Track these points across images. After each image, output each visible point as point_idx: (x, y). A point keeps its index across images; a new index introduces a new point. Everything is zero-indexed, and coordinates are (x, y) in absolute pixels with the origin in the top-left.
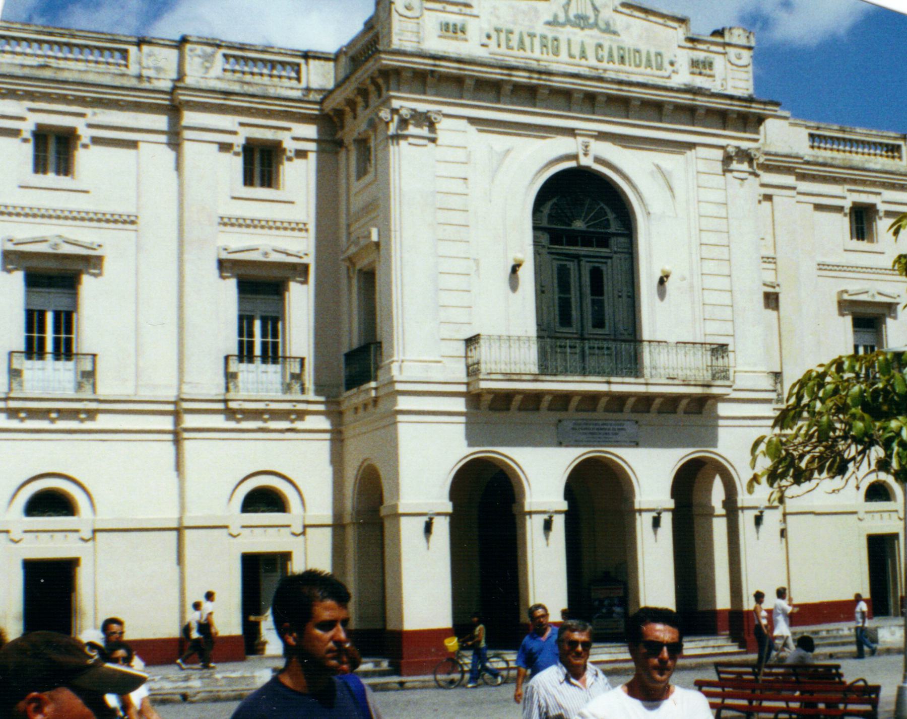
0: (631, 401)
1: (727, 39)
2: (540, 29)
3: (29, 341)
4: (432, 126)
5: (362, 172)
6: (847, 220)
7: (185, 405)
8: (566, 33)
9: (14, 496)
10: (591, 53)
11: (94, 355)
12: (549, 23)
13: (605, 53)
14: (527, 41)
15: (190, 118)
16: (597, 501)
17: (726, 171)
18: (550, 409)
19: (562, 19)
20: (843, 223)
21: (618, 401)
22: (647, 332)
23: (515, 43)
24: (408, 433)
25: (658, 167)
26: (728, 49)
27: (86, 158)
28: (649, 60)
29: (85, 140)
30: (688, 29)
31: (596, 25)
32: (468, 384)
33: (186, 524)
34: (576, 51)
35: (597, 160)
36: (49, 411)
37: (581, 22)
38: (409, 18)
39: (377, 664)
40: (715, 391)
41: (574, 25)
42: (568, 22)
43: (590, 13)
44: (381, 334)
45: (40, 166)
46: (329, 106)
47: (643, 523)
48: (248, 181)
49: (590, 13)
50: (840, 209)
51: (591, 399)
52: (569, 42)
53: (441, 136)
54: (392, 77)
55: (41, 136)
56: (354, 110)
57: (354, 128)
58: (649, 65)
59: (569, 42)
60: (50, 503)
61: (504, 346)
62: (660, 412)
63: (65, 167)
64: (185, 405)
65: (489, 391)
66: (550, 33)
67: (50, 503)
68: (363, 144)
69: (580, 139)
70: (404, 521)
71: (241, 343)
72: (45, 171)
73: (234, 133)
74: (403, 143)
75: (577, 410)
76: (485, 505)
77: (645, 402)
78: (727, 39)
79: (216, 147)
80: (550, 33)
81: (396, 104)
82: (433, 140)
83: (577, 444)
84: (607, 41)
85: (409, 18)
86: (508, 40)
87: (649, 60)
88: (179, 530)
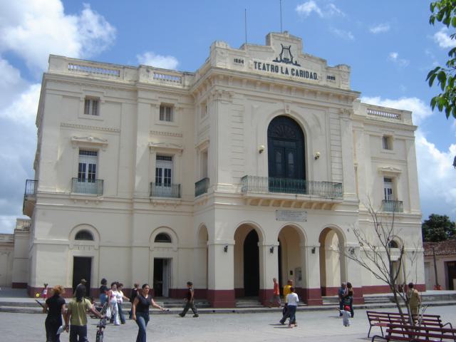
0: (261, 201)
1: (340, 69)
2: (271, 63)
3: (80, 175)
4: (230, 96)
5: (203, 115)
6: (382, 141)
7: (136, 200)
8: (280, 65)
9: (77, 226)
10: (290, 72)
11: (103, 181)
12: (274, 61)
13: (295, 72)
14: (266, 66)
15: (141, 94)
16: (290, 239)
17: (339, 119)
18: (273, 206)
19: (279, 59)
20: (381, 142)
21: (300, 204)
22: (310, 177)
23: (261, 67)
24: (218, 213)
25: (314, 115)
26: (341, 73)
27: (103, 108)
28: (311, 75)
29: (103, 102)
30: (326, 64)
31: (291, 62)
32: (242, 195)
33: (134, 245)
34: (284, 71)
35: (292, 111)
36: (85, 200)
37: (286, 61)
38: (173, 230)
39: (204, 303)
40: (334, 201)
41: (283, 62)
42: (281, 61)
43: (289, 57)
44: (210, 176)
45: (86, 112)
46: (192, 91)
47: (308, 251)
48: (161, 118)
49: (289, 57)
50: (379, 137)
51: (289, 203)
52: (282, 68)
53: (234, 101)
54: (216, 77)
55: (87, 101)
56: (201, 92)
57: (201, 99)
58: (311, 77)
59: (282, 68)
60: (84, 235)
61: (261, 181)
62: (315, 208)
63: (96, 112)
64: (136, 200)
65: (250, 197)
66: (275, 64)
67: (84, 235)
68: (204, 104)
69: (286, 104)
70: (216, 247)
71: (157, 179)
72: (88, 113)
73: (157, 100)
74: (219, 103)
75: (284, 206)
76: (249, 243)
77: (310, 204)
78: (340, 69)
79: (149, 105)
80: (275, 64)
81: (217, 88)
82: (231, 102)
83: (283, 219)
84: (296, 67)
85: (173, 230)
86: (259, 66)
87: (311, 75)
88: (131, 247)
